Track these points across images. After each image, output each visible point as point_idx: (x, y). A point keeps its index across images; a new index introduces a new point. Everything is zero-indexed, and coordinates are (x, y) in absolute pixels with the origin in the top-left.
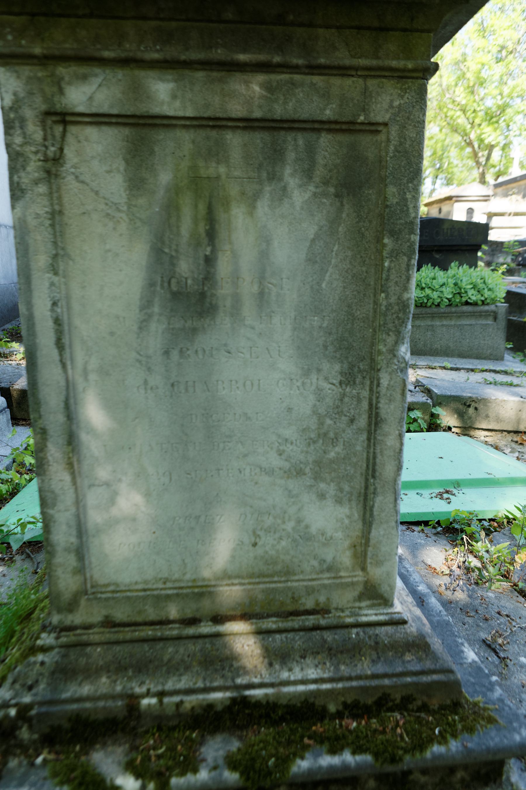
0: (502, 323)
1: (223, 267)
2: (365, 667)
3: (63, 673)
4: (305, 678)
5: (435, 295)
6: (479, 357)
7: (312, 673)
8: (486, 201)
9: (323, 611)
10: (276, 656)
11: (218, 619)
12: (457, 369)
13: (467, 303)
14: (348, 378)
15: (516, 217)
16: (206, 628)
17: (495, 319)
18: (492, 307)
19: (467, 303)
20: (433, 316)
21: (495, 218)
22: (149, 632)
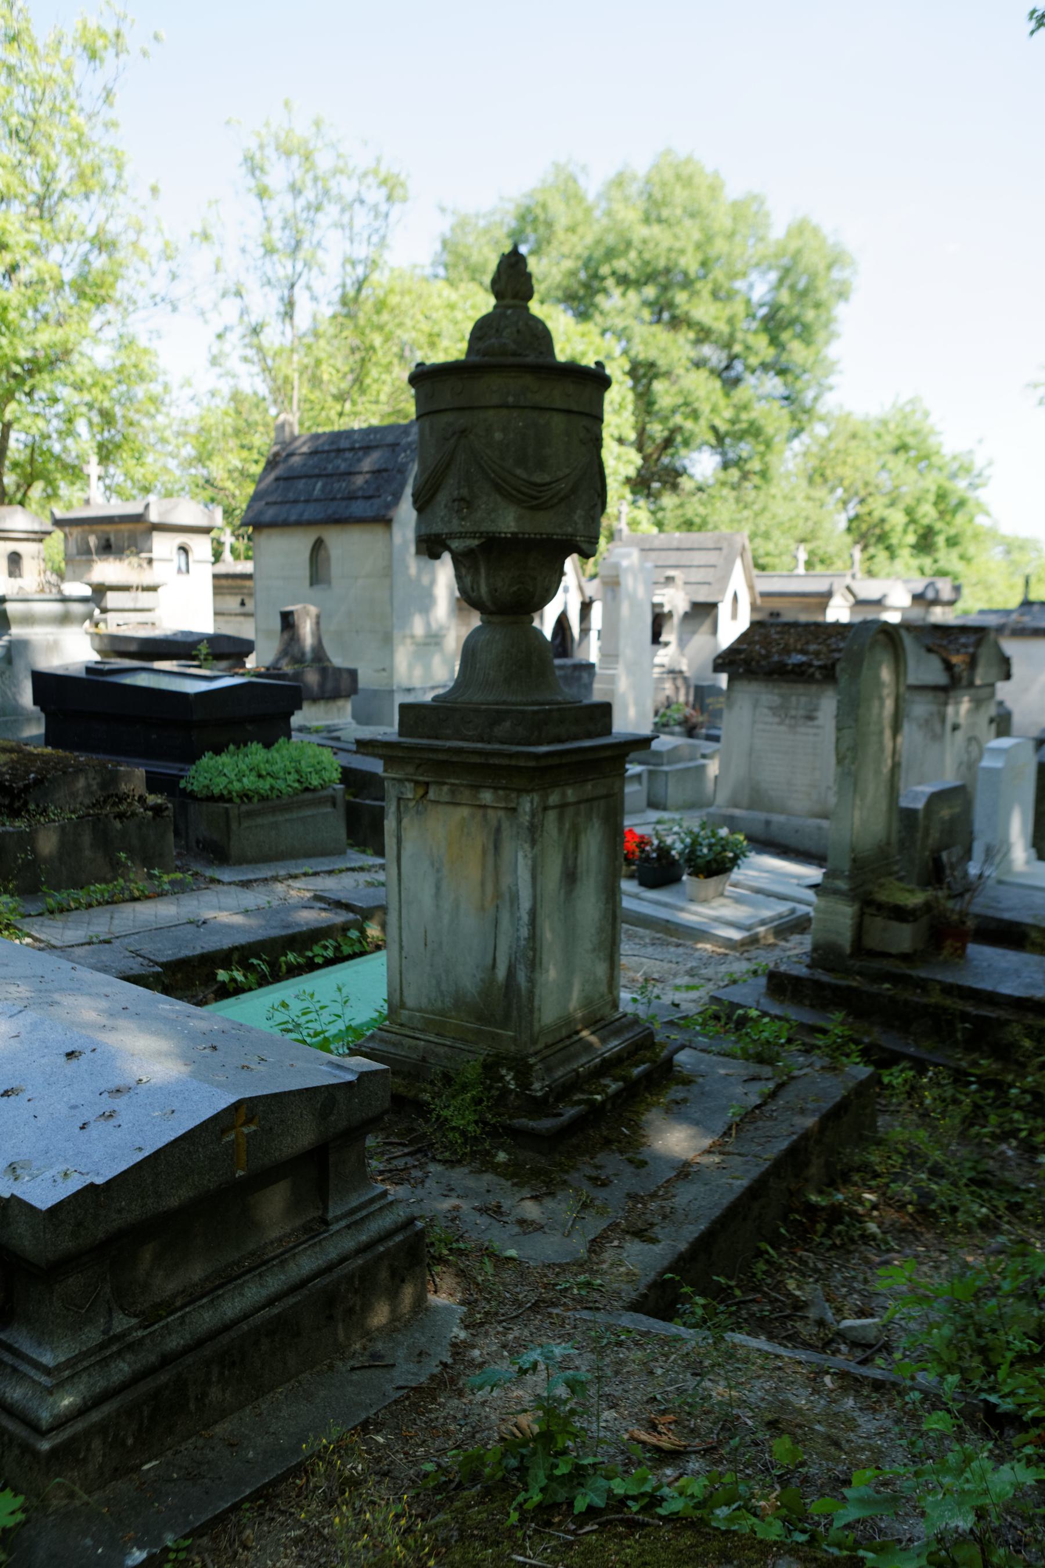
0: (341, 809)
1: (579, 862)
2: (628, 1035)
3: (549, 1070)
4: (615, 1044)
5: (280, 785)
6: (324, 853)
7: (616, 1043)
8: (41, 540)
9: (602, 1019)
10: (603, 1040)
11: (577, 1032)
12: (316, 874)
13: (307, 789)
14: (607, 903)
15: (145, 594)
16: (576, 1038)
17: (334, 805)
18: (330, 792)
19: (307, 789)
20: (274, 810)
21: (110, 595)
22: (560, 1046)
